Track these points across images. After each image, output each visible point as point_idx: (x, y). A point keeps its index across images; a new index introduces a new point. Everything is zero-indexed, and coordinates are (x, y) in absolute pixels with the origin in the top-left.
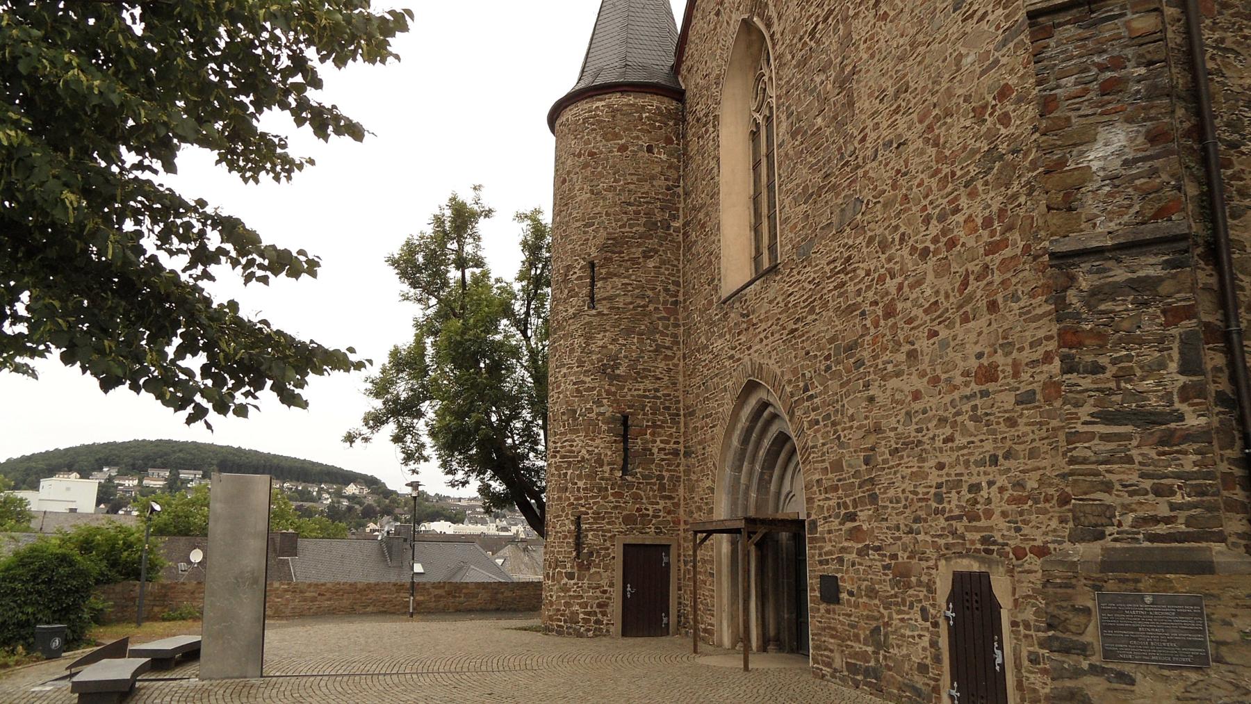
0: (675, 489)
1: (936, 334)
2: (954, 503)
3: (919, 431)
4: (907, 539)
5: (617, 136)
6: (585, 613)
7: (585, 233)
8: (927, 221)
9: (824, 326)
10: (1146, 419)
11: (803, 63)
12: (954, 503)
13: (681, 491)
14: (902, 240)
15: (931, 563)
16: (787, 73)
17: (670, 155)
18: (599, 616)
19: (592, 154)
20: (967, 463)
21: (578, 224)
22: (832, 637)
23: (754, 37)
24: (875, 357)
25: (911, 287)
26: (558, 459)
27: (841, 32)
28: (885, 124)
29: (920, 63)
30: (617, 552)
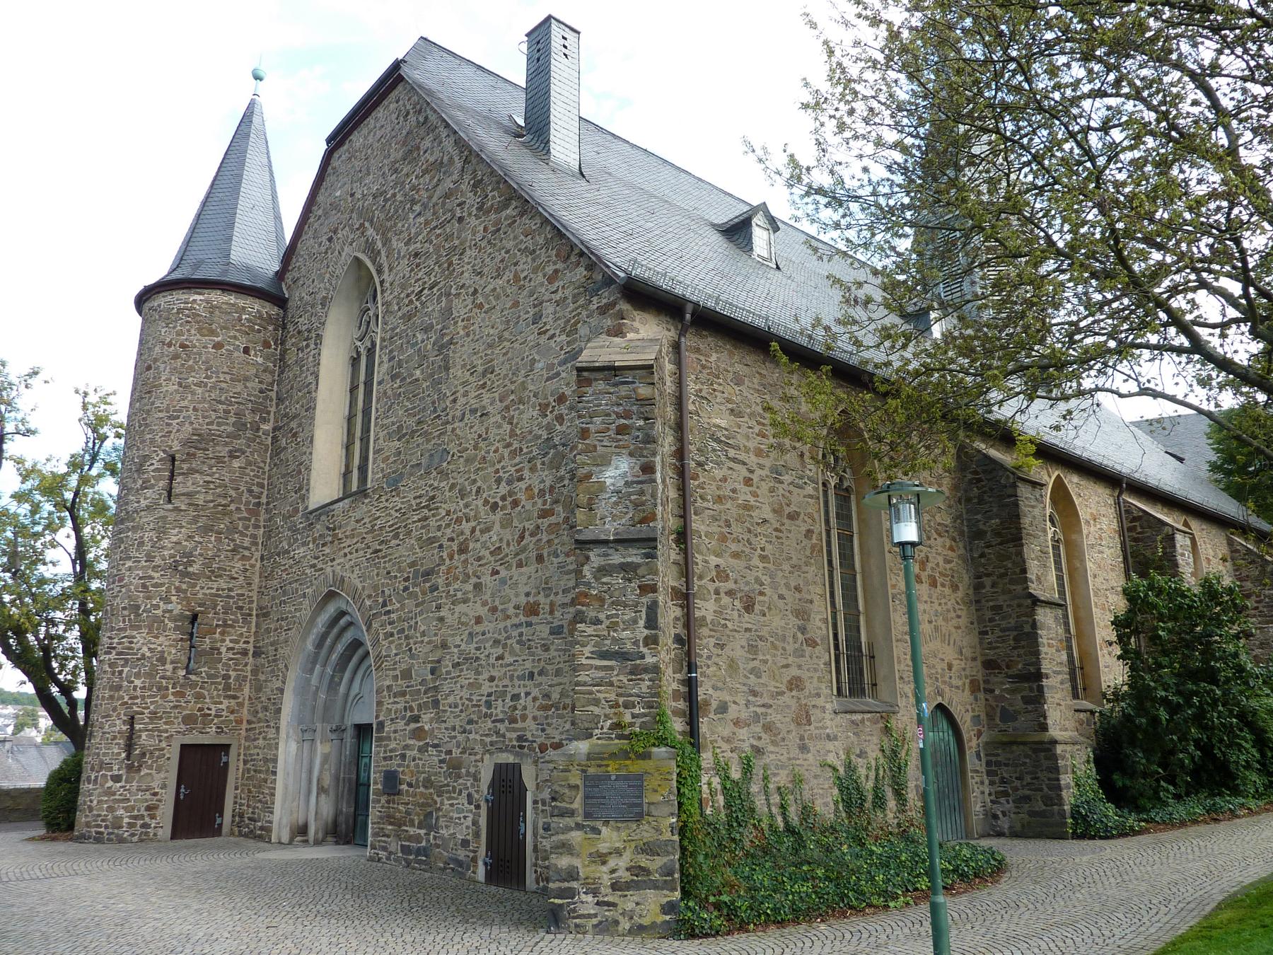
0: (240, 689)
1: (497, 573)
2: (499, 709)
3: (478, 649)
4: (461, 738)
5: (213, 333)
6: (130, 817)
7: (168, 424)
8: (499, 481)
9: (406, 551)
10: (623, 656)
11: (408, 317)
12: (499, 709)
13: (246, 691)
14: (478, 492)
15: (478, 757)
16: (393, 321)
17: (267, 358)
18: (147, 820)
19: (183, 346)
20: (512, 677)
21: (161, 415)
22: (391, 824)
23: (363, 273)
24: (448, 585)
25: (482, 532)
26: (113, 656)
27: (443, 304)
28: (473, 394)
29: (505, 354)
30: (174, 754)
